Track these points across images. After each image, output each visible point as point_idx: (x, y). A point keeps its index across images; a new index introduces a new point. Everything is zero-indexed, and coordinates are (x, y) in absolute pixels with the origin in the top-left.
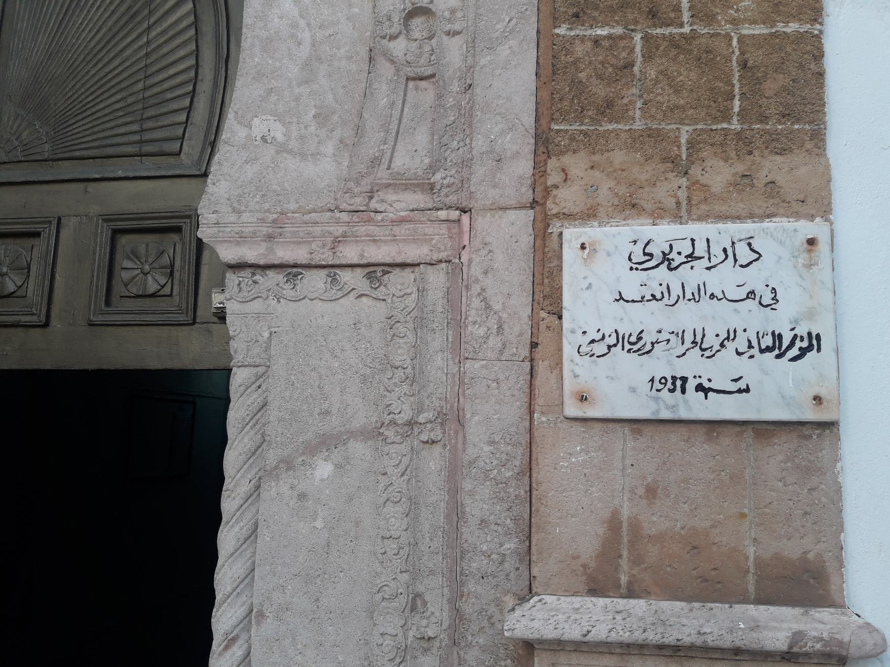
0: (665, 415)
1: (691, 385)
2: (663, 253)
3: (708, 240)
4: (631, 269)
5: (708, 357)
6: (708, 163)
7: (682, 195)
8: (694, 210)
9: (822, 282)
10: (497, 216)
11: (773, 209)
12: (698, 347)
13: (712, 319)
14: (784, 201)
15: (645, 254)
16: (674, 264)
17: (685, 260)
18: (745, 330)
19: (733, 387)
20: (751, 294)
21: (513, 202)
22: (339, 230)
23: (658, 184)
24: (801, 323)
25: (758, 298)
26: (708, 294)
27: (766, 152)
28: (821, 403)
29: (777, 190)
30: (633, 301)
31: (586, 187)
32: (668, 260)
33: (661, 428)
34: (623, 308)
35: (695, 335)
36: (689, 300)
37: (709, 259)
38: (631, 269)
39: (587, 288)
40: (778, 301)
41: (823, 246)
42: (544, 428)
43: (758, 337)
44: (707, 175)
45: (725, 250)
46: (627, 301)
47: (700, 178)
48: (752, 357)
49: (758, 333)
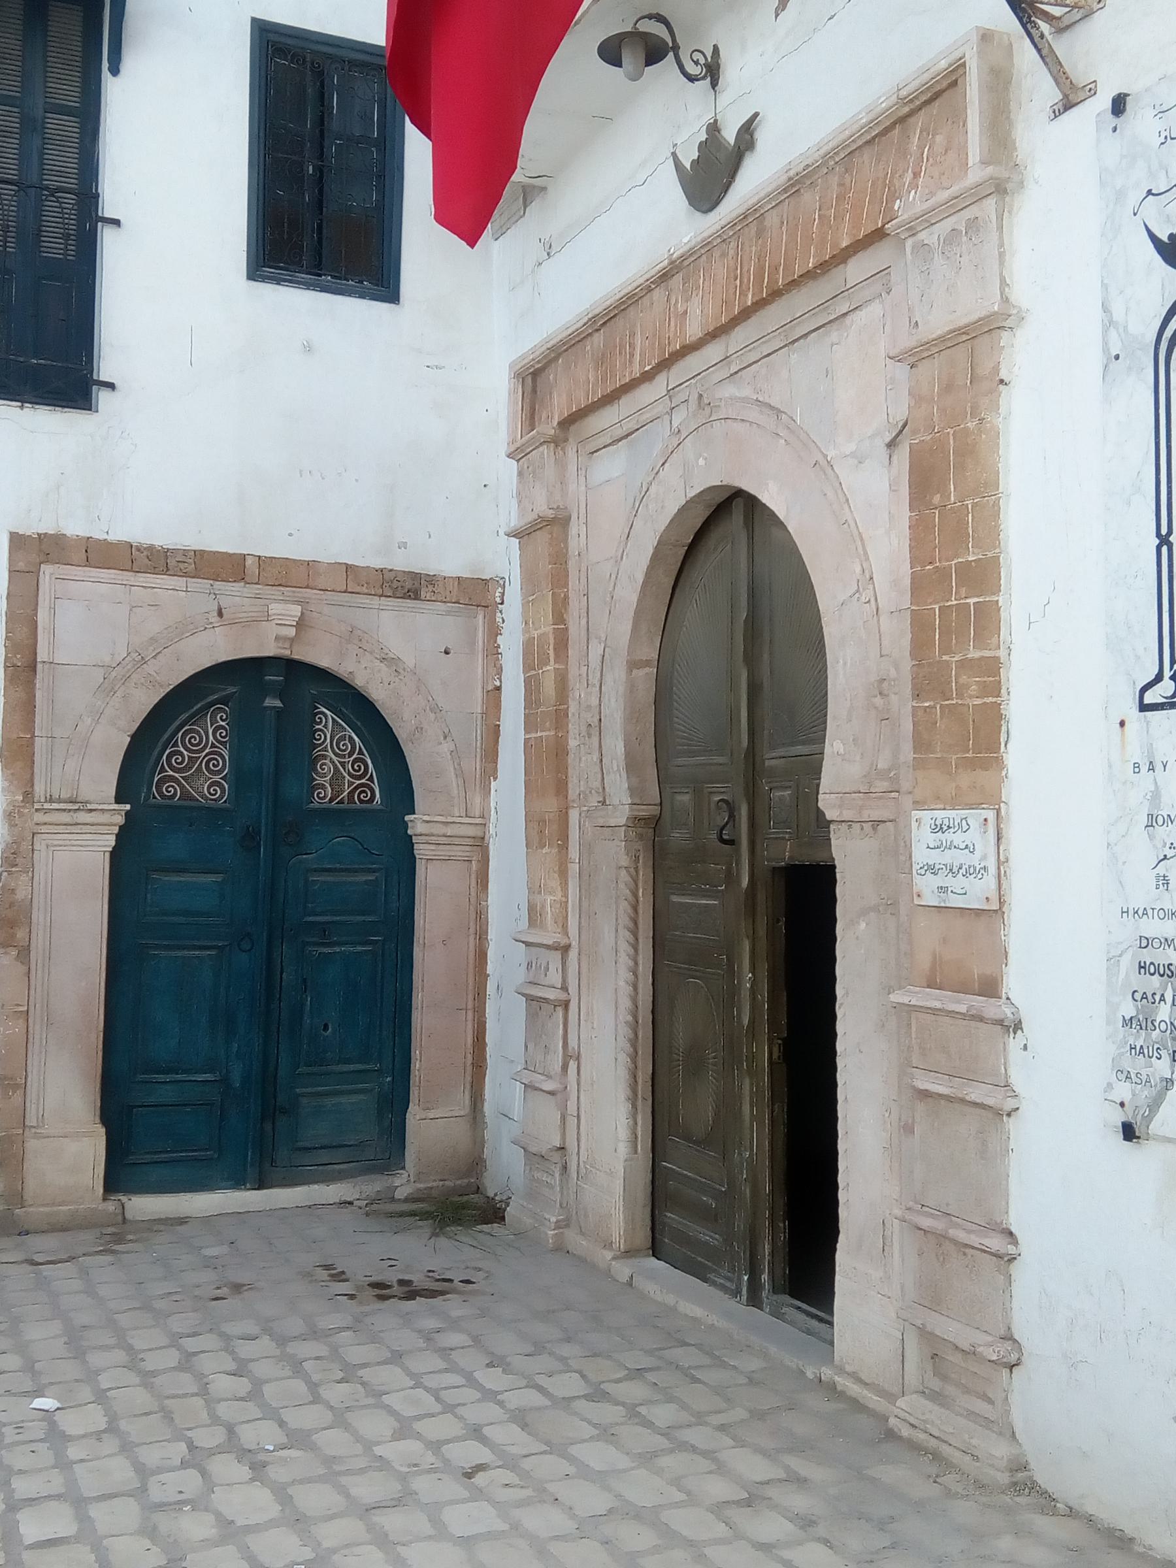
22: (860, 803)
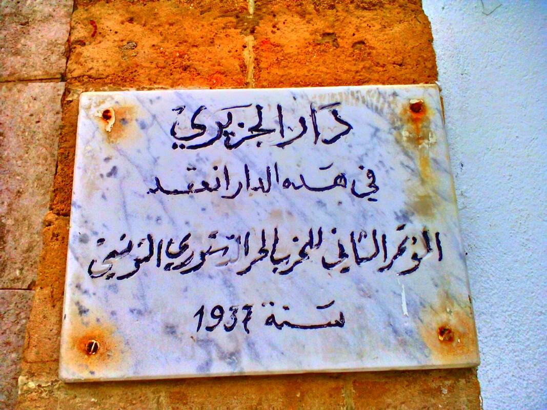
0: (220, 369)
1: (260, 314)
2: (219, 124)
3: (279, 108)
4: (175, 146)
5: (283, 273)
6: (280, 19)
7: (248, 56)
8: (264, 74)
9: (435, 161)
10: (15, 90)
11: (365, 75)
12: (268, 258)
13: (292, 216)
14: (377, 64)
15: (194, 126)
16: (234, 140)
17: (250, 134)
18: (334, 231)
19: (318, 318)
20: (340, 180)
21: (39, 73)
23: (217, 42)
24: (412, 218)
25: (349, 185)
26: (282, 180)
27: (351, 6)
28: (451, 339)
29: (368, 51)
30: (176, 192)
31: (121, 44)
32: (226, 134)
33: (217, 389)
34: (161, 202)
35: (264, 240)
36: (256, 189)
37: (282, 132)
38: (175, 146)
39: (110, 175)
40: (377, 188)
41: (433, 115)
42: (32, 400)
43: (353, 240)
44: (278, 33)
45: (302, 121)
46: (168, 192)
47: (271, 35)
48: (345, 270)
49: (352, 234)
